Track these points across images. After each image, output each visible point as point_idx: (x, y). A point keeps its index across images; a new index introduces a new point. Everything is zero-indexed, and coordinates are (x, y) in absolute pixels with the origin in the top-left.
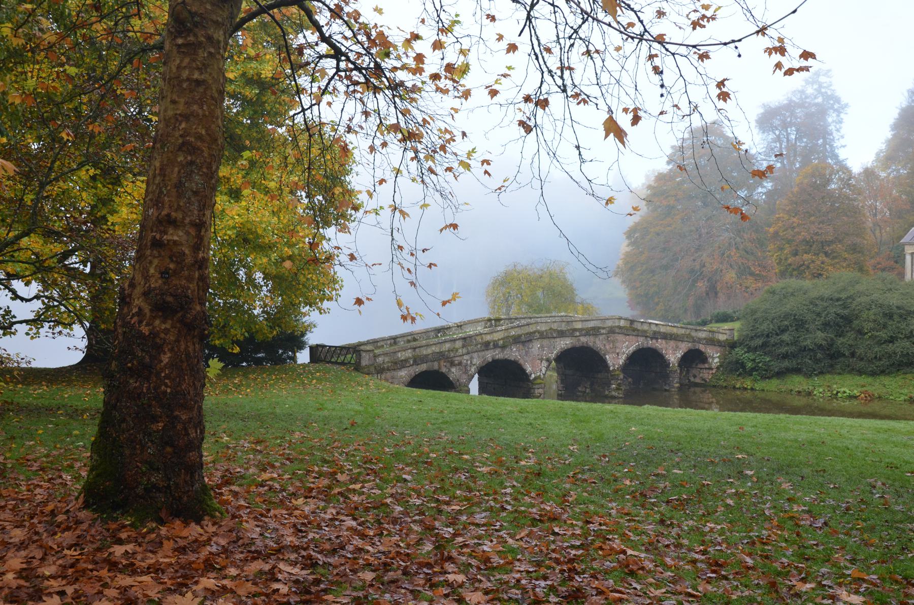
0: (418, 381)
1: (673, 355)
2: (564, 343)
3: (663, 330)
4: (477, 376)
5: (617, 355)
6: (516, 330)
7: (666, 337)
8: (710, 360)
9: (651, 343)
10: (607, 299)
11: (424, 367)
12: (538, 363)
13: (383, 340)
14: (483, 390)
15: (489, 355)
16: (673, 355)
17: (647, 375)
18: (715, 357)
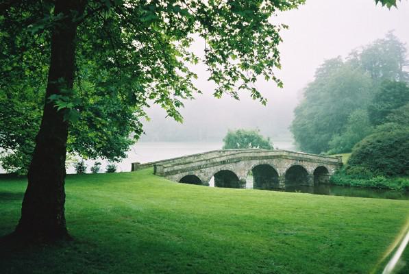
0: (183, 180)
1: (310, 169)
2: (255, 163)
3: (305, 156)
4: (213, 178)
5: (282, 168)
6: (183, 166)
7: (306, 160)
8: (329, 171)
9: (299, 163)
10: (285, 144)
11: (187, 173)
12: (244, 172)
13: (169, 160)
14: (218, 184)
15: (219, 168)
16: (310, 169)
17: (297, 179)
18: (332, 170)
